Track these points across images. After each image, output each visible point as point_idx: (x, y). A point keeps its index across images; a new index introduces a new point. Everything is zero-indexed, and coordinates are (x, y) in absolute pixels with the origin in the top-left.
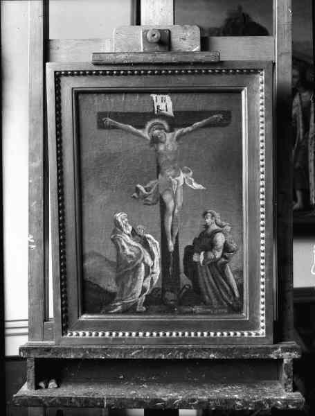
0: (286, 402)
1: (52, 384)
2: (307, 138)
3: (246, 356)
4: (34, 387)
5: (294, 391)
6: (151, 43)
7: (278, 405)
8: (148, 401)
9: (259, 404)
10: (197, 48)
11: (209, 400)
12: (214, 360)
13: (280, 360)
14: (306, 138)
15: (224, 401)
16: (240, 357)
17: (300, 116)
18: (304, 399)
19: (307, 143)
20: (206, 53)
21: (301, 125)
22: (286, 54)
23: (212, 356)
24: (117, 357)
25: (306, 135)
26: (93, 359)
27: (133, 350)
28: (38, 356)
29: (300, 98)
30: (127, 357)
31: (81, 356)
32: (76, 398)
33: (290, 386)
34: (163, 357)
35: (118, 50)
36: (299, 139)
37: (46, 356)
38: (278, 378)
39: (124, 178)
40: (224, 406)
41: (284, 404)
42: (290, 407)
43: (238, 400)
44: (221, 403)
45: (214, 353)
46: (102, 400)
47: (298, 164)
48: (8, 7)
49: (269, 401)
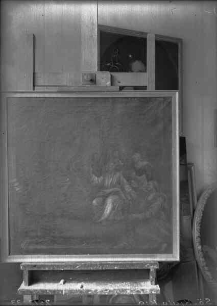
0: (151, 290)
1: (62, 282)
3: (132, 268)
6: (87, 81)
10: (109, 83)
11: (114, 290)
12: (116, 270)
13: (149, 270)
18: (117, 303)
20: (112, 87)
23: (116, 268)
24: (69, 269)
26: (58, 271)
27: (77, 265)
28: (29, 269)
30: (75, 269)
31: (51, 269)
32: (49, 290)
33: (153, 282)
34: (92, 269)
35: (71, 84)
37: (33, 269)
38: (149, 279)
39: (131, 196)
42: (153, 292)
43: (128, 290)
45: (117, 266)
46: (62, 291)
49: (143, 290)
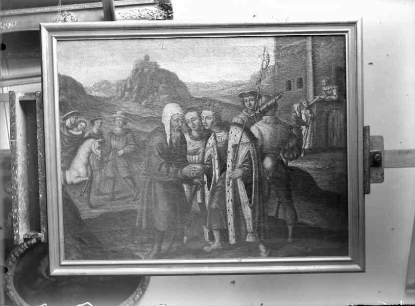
0: (18, 235)
2: (224, 178)
4: (21, 100)
5: (24, 239)
7: (16, 230)
8: (15, 163)
9: (16, 221)
12: (39, 196)
14: (223, 179)
15: (16, 203)
16: (41, 210)
17: (216, 156)
19: (224, 183)
21: (217, 166)
22: (88, 44)
25: (222, 176)
29: (215, 138)
33: (27, 237)
36: (215, 178)
40: (14, 203)
41: (17, 234)
42: (15, 237)
43: (17, 210)
44: (16, 201)
47: (214, 205)
48: (414, 303)
49: (18, 226)
